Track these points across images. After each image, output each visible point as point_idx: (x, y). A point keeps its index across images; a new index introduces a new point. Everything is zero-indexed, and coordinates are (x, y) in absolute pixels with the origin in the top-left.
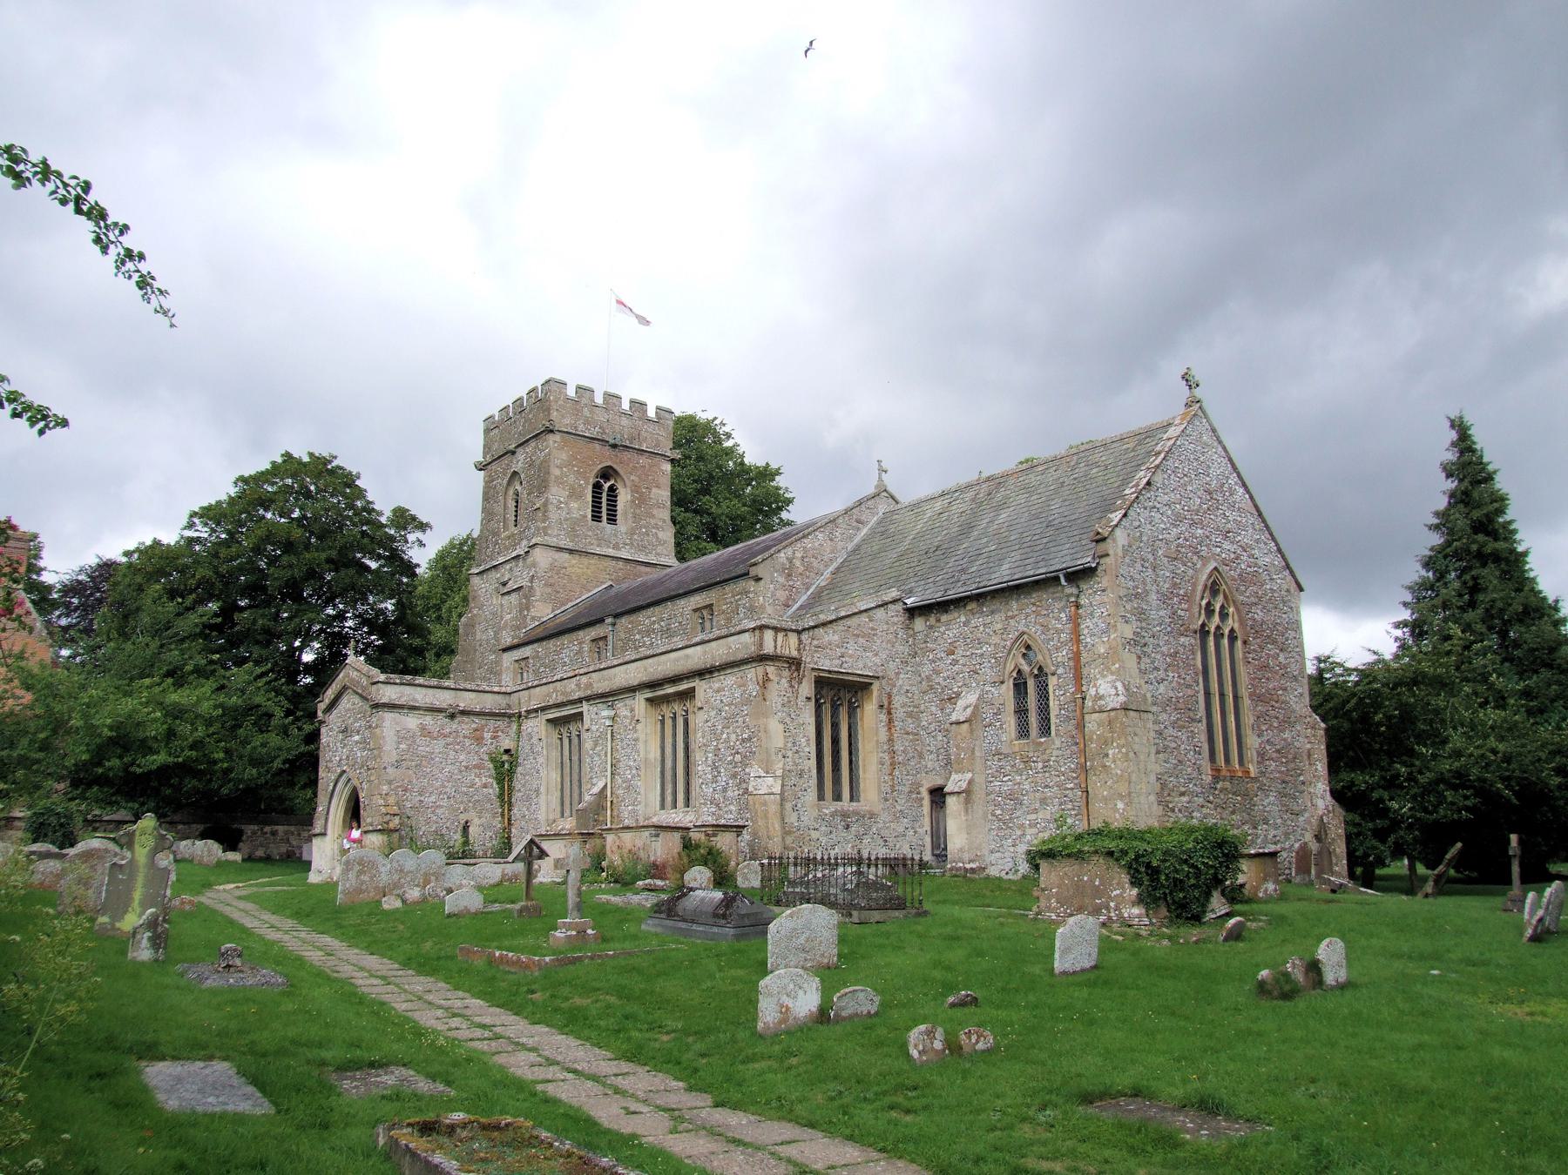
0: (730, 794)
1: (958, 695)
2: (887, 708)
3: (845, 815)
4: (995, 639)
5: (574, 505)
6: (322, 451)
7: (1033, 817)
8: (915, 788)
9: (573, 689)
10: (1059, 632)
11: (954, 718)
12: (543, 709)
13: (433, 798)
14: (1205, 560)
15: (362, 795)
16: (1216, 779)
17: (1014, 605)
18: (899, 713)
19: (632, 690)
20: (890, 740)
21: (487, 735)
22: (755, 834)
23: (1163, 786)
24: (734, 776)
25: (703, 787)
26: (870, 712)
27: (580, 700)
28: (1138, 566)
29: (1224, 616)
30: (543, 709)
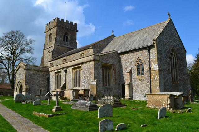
0: (87, 84)
1: (127, 68)
2: (115, 70)
3: (107, 88)
4: (134, 58)
5: (61, 38)
6: (18, 30)
7: (141, 89)
8: (119, 84)
9: (59, 67)
10: (146, 57)
11: (126, 72)
12: (54, 70)
13: (35, 85)
14: (171, 45)
15: (22, 85)
16: (173, 83)
17: (138, 52)
18: (117, 71)
19: (69, 67)
20: (115, 76)
21: (45, 75)
22: (91, 91)
23: (164, 84)
24: (88, 81)
25: (82, 83)
26: (112, 71)
27: (60, 69)
28: (161, 45)
29: (174, 55)
30: (54, 70)
